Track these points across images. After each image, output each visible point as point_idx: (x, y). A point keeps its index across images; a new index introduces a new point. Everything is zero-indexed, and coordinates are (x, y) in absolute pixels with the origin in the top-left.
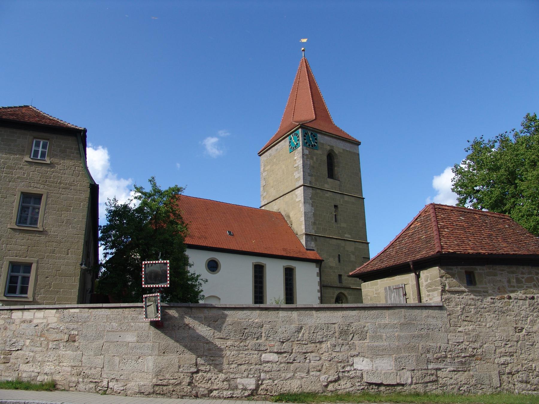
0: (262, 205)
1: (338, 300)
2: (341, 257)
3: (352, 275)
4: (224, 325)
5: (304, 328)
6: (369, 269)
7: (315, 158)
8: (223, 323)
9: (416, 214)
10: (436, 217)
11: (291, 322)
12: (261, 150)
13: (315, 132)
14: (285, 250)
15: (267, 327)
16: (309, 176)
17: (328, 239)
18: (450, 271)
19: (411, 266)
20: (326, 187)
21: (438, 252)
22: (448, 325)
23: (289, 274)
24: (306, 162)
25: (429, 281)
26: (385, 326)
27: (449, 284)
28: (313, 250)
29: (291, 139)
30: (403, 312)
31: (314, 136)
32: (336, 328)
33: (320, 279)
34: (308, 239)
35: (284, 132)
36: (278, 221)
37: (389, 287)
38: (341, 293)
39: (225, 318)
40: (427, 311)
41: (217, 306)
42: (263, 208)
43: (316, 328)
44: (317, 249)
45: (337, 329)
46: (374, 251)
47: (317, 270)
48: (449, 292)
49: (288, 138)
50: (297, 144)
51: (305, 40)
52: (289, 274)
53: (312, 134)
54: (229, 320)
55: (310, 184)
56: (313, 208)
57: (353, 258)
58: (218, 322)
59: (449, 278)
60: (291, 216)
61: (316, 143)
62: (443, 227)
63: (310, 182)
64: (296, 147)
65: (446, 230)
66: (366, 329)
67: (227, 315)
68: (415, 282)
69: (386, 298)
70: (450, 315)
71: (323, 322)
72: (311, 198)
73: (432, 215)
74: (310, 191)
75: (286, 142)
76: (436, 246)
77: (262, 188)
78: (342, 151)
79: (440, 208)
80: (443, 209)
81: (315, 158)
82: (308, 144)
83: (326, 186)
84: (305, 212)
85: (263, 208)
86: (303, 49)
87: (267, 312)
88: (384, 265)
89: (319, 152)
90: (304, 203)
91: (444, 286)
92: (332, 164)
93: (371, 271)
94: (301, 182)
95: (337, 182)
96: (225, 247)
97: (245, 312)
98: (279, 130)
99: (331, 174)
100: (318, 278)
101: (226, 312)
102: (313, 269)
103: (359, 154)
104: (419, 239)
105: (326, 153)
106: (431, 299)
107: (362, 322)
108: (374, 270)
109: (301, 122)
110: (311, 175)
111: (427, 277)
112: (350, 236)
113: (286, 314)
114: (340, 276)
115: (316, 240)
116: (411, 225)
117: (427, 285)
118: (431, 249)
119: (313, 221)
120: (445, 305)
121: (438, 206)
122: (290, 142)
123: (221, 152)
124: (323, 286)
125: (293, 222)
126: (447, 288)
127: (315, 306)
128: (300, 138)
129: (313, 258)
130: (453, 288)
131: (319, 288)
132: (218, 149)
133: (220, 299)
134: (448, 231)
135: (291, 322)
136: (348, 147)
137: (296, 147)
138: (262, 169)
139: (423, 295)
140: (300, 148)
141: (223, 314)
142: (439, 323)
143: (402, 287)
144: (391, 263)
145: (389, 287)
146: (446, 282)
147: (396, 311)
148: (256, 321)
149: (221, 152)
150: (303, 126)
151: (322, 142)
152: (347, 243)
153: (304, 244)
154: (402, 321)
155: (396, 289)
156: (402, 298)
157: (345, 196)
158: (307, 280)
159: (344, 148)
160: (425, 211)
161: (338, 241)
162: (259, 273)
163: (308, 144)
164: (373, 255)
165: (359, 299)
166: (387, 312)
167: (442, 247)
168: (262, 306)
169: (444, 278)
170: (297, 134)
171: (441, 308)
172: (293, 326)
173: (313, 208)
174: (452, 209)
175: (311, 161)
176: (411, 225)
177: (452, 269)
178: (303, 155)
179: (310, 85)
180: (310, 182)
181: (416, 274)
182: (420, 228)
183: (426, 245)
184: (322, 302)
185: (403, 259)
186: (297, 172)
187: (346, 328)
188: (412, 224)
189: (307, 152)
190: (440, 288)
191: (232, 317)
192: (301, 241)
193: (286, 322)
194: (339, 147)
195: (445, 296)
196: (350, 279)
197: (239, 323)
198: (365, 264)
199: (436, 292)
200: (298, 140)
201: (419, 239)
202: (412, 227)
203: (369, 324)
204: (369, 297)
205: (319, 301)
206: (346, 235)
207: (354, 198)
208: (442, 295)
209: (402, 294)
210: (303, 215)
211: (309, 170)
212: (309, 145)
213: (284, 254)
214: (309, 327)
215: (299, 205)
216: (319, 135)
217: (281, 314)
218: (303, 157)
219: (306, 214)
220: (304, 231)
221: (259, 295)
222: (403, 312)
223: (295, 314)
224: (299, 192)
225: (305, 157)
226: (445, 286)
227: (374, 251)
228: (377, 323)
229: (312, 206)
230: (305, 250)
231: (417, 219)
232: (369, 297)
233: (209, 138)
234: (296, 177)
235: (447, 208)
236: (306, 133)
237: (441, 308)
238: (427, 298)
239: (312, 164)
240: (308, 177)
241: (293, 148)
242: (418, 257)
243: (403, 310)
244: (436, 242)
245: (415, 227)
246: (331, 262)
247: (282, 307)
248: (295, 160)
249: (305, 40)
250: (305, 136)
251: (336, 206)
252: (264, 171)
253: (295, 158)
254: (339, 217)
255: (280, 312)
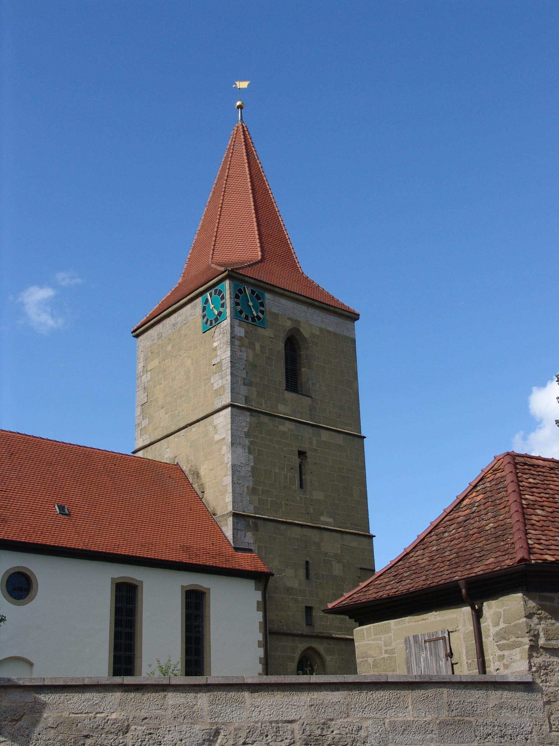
0: (137, 447)
1: (305, 664)
2: (311, 567)
3: (333, 608)
4: (38, 729)
5: (222, 733)
6: (371, 595)
7: (258, 347)
8: (35, 723)
9: (473, 475)
10: (518, 482)
11: (193, 717)
12: (139, 324)
13: (261, 288)
14: (186, 549)
15: (137, 730)
16: (244, 384)
17: (283, 527)
18: (548, 604)
19: (464, 591)
20: (282, 410)
21: (522, 560)
22: (546, 728)
23: (195, 606)
24: (238, 353)
25: (502, 625)
26: (406, 727)
27: (546, 631)
28: (250, 551)
29: (207, 301)
30: (445, 696)
31: (258, 298)
32: (296, 732)
33: (265, 617)
34: (239, 527)
35: (192, 287)
36: (172, 483)
37: (415, 637)
38: (310, 648)
39: (40, 713)
40: (499, 693)
41: (21, 683)
42: (140, 454)
43: (251, 732)
44: (259, 547)
45: (298, 735)
46: (384, 556)
47: (258, 596)
48: (546, 650)
49: (200, 301)
50: (220, 314)
51: (243, 85)
52: (195, 606)
53: (253, 292)
54: (49, 716)
55: (246, 402)
56: (251, 457)
57: (337, 569)
58: (23, 723)
59: (546, 618)
60: (202, 473)
61: (262, 312)
62: (532, 506)
63: (246, 398)
64: (216, 320)
65: (539, 512)
66: (363, 733)
67: (44, 705)
68: (470, 628)
69: (408, 662)
70: (548, 702)
71: (267, 718)
72: (247, 435)
73: (510, 478)
74: (246, 418)
75: (194, 307)
76: (517, 546)
77: (138, 411)
78: (317, 333)
79: (525, 464)
80: (533, 465)
81: (258, 347)
82: (243, 315)
83: (281, 407)
84: (233, 466)
85: (140, 454)
86: (238, 103)
87: (139, 695)
88: (405, 586)
89: (268, 333)
90: (233, 444)
91: (534, 636)
92: (295, 361)
93: (375, 600)
94: (227, 399)
95: (306, 401)
96: (50, 541)
97: (88, 695)
98: (180, 280)
99: (293, 382)
100: (261, 614)
101: (43, 697)
102: (248, 595)
103: (354, 341)
104: (481, 529)
105: (283, 336)
106: (506, 667)
107: (354, 719)
108: (381, 599)
109: (231, 265)
110: (248, 383)
111: (498, 616)
112: (331, 520)
113: (183, 700)
114: (309, 610)
115: (256, 528)
116: (463, 500)
117: (497, 634)
118: (506, 552)
119: (251, 484)
120: (538, 681)
121: (522, 460)
122: (204, 309)
123: (61, 321)
124: (271, 633)
125: (206, 486)
126: (542, 641)
127: (249, 681)
128: (228, 301)
129: (249, 568)
130: (554, 642)
131: (260, 637)
132: (52, 315)
133: (31, 664)
134: (544, 513)
135: (193, 717)
136: (330, 323)
137: (216, 320)
138: (140, 366)
139: (489, 657)
140: (226, 324)
141: (35, 702)
142: (527, 723)
143: (443, 638)
144: (419, 582)
145: (415, 637)
146: (540, 628)
147: (430, 692)
148: (114, 716)
149: (61, 321)
150: (234, 275)
151: (275, 310)
152: (326, 534)
153: (232, 542)
154: (444, 715)
155: (430, 641)
156: (443, 663)
157: (324, 433)
158: (237, 625)
159: (323, 326)
160: (494, 470)
161: (305, 531)
162: (126, 600)
163: (243, 315)
164: (381, 563)
165: (350, 665)
166: (410, 696)
167: (530, 549)
168: (128, 680)
169: (535, 620)
170: (220, 292)
171: (528, 686)
172: (198, 727)
173: (251, 457)
174: (552, 465)
175: (250, 351)
176: (463, 500)
177: (551, 600)
178: (232, 338)
179: (252, 185)
180: (247, 399)
181: (473, 608)
182: (482, 507)
183: (495, 545)
184: (267, 671)
185: (446, 575)
186: (217, 376)
187: (318, 732)
188: (466, 496)
189: (240, 332)
190: (526, 641)
191: (57, 707)
192: (224, 529)
193: (183, 715)
194: (312, 322)
195: (538, 660)
196: (331, 616)
197: (74, 723)
198: (363, 585)
199: (518, 650)
200: (223, 305)
201: (481, 529)
202: (465, 503)
203: (370, 722)
204: (370, 660)
205: (260, 668)
206: (323, 519)
207: (341, 436)
208: (530, 657)
209: (442, 654)
210: (230, 473)
211: (244, 372)
212: (247, 317)
213: (184, 558)
214: (235, 729)
215: (220, 450)
216: (268, 296)
217: (173, 699)
218: (232, 343)
219: (235, 469)
220: (230, 508)
221: (124, 655)
222: (445, 696)
223: (203, 700)
224: (222, 419)
225: (237, 343)
226: (537, 636)
227: (384, 556)
228: (387, 721)
229: (250, 453)
230: (231, 551)
231: (475, 486)
232: (370, 660)
233: (33, 289)
234: (216, 387)
235: (541, 462)
236: (240, 291)
237: (528, 686)
238: (497, 664)
239: (251, 359)
240: (242, 387)
241: (211, 323)
242: (479, 570)
243: (445, 690)
244: (516, 537)
245: (472, 504)
246: (289, 578)
247: (173, 682)
248: (215, 349)
249: (243, 85)
250: (237, 297)
251: (302, 454)
252: (145, 370)
253: (215, 344)
254: (307, 477)
255: (170, 695)
